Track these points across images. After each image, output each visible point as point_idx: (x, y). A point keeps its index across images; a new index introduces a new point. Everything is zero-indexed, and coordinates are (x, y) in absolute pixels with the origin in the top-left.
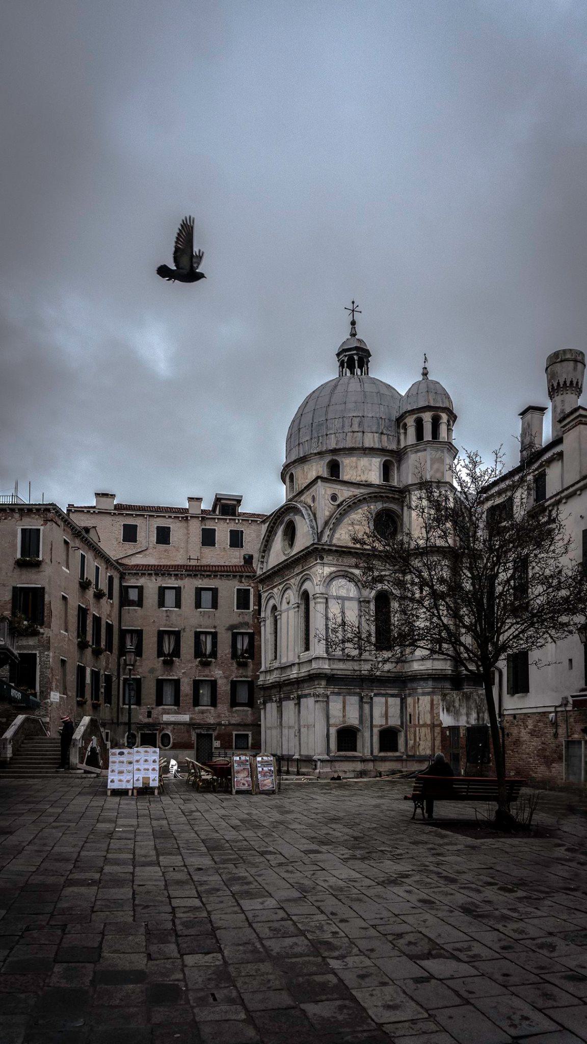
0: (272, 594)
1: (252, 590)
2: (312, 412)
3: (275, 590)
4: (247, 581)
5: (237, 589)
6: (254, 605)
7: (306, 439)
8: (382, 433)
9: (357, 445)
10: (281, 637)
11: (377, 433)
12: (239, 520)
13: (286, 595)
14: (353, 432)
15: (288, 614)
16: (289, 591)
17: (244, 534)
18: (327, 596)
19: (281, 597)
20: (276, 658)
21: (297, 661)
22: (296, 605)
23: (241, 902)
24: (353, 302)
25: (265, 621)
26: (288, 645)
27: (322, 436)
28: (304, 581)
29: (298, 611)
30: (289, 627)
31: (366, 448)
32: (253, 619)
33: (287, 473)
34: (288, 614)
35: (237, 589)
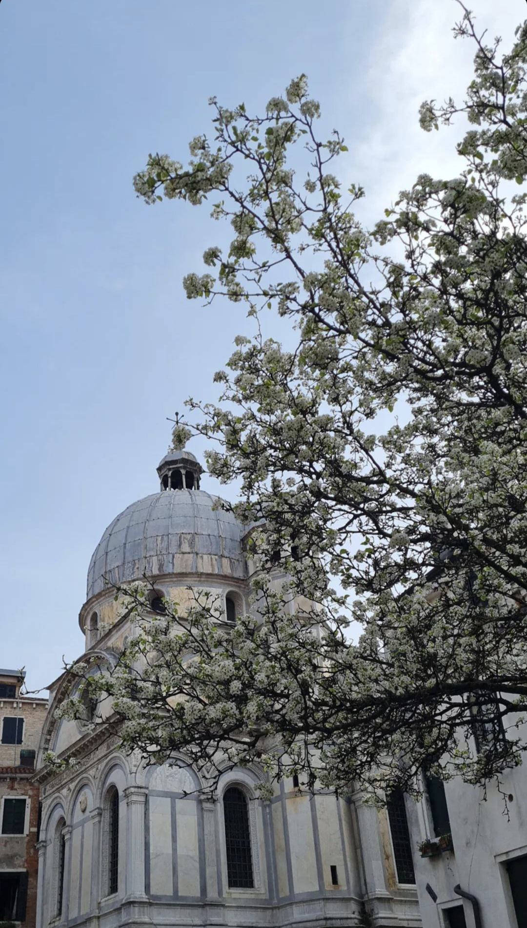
0: (58, 799)
1: (29, 801)
2: (125, 530)
3: (65, 791)
4: (22, 786)
5: (6, 800)
6: (31, 825)
7: (116, 565)
8: (222, 556)
9: (189, 570)
10: (69, 871)
11: (215, 555)
12: (17, 702)
13: (81, 798)
14: (183, 553)
15: (79, 911)
16: (86, 790)
17: (24, 724)
18: (147, 791)
19: (72, 802)
20: (60, 914)
21: (96, 913)
22: (96, 812)
23: (250, 574)
24: (177, 414)
25: (45, 847)
26: (80, 884)
27: (139, 559)
28: (111, 769)
29: (100, 822)
30: (84, 853)
31: (202, 574)
32: (28, 849)
33: (88, 613)
34: (79, 911)
35: (6, 800)
